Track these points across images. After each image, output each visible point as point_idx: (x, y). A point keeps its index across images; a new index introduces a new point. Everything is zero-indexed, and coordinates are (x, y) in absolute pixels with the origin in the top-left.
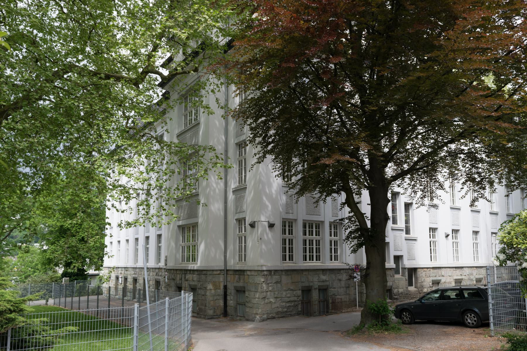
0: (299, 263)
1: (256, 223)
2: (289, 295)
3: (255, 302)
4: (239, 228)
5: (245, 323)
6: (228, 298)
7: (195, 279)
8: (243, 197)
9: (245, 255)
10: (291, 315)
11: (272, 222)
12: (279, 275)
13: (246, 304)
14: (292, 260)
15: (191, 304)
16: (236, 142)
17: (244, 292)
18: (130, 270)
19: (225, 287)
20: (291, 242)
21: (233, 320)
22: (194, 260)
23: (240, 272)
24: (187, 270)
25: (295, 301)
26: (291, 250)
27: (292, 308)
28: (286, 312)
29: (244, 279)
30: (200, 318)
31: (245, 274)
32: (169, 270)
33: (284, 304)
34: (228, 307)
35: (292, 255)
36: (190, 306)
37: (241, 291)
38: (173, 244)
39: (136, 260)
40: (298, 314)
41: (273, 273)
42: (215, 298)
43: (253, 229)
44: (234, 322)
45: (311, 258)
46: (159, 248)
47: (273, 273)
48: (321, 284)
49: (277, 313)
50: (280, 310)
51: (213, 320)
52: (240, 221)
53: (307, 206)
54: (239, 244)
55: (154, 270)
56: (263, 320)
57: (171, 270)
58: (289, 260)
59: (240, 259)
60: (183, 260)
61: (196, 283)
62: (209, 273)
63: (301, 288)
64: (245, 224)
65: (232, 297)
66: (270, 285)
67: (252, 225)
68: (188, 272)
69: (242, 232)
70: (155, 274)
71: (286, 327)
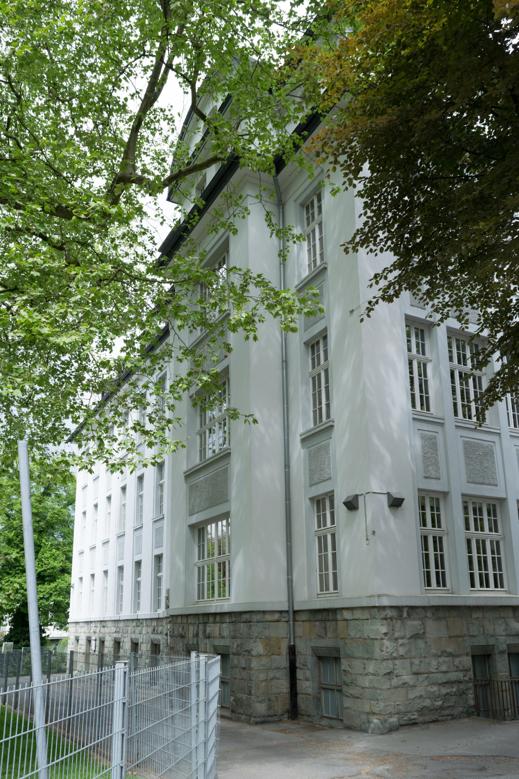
0: (461, 590)
1: (361, 499)
2: (444, 668)
3: (367, 685)
4: (319, 517)
5: (344, 736)
6: (299, 674)
7: (226, 633)
8: (326, 448)
9: (335, 575)
10: (453, 717)
11: (396, 493)
12: (419, 619)
13: (345, 689)
14: (444, 585)
15: (215, 688)
16: (305, 340)
17: (337, 659)
18: (110, 624)
19: (292, 651)
20: (438, 542)
21: (312, 727)
22: (224, 589)
23: (326, 615)
24: (207, 615)
25: (460, 682)
26: (440, 562)
27: (453, 699)
28: (441, 708)
29: (336, 630)
30: (238, 720)
31: (339, 617)
32: (173, 618)
33: (435, 688)
34: (299, 697)
35: (443, 573)
36: (211, 695)
37: (329, 658)
38: (180, 564)
39: (119, 607)
40: (469, 714)
41: (405, 615)
42: (271, 675)
43: (353, 513)
44: (316, 734)
45: (484, 582)
46: (158, 580)
47: (405, 615)
48: (512, 641)
49: (422, 711)
50: (427, 703)
51: (266, 726)
52: (321, 503)
53: (467, 464)
54: (320, 551)
55: (148, 623)
56: (392, 730)
57: (177, 616)
58: (438, 584)
59: (324, 586)
60: (201, 595)
61: (227, 642)
62: (255, 618)
63: (469, 650)
64: (332, 506)
65: (308, 673)
66: (400, 641)
67: (352, 505)
68: (211, 619)
69: (325, 525)
70: (150, 630)
71: (460, 751)
